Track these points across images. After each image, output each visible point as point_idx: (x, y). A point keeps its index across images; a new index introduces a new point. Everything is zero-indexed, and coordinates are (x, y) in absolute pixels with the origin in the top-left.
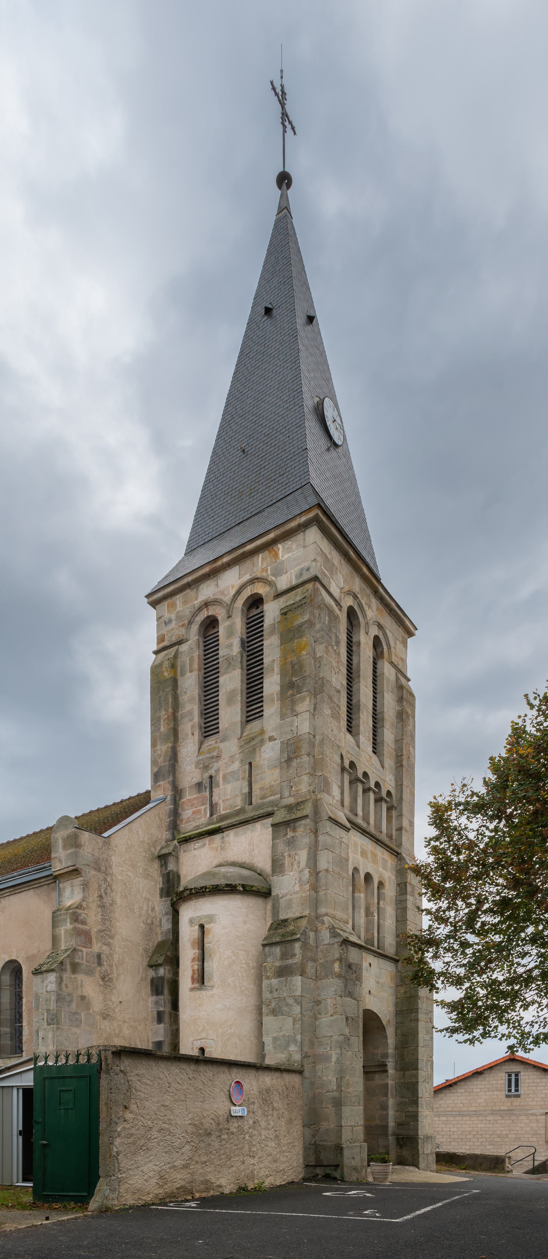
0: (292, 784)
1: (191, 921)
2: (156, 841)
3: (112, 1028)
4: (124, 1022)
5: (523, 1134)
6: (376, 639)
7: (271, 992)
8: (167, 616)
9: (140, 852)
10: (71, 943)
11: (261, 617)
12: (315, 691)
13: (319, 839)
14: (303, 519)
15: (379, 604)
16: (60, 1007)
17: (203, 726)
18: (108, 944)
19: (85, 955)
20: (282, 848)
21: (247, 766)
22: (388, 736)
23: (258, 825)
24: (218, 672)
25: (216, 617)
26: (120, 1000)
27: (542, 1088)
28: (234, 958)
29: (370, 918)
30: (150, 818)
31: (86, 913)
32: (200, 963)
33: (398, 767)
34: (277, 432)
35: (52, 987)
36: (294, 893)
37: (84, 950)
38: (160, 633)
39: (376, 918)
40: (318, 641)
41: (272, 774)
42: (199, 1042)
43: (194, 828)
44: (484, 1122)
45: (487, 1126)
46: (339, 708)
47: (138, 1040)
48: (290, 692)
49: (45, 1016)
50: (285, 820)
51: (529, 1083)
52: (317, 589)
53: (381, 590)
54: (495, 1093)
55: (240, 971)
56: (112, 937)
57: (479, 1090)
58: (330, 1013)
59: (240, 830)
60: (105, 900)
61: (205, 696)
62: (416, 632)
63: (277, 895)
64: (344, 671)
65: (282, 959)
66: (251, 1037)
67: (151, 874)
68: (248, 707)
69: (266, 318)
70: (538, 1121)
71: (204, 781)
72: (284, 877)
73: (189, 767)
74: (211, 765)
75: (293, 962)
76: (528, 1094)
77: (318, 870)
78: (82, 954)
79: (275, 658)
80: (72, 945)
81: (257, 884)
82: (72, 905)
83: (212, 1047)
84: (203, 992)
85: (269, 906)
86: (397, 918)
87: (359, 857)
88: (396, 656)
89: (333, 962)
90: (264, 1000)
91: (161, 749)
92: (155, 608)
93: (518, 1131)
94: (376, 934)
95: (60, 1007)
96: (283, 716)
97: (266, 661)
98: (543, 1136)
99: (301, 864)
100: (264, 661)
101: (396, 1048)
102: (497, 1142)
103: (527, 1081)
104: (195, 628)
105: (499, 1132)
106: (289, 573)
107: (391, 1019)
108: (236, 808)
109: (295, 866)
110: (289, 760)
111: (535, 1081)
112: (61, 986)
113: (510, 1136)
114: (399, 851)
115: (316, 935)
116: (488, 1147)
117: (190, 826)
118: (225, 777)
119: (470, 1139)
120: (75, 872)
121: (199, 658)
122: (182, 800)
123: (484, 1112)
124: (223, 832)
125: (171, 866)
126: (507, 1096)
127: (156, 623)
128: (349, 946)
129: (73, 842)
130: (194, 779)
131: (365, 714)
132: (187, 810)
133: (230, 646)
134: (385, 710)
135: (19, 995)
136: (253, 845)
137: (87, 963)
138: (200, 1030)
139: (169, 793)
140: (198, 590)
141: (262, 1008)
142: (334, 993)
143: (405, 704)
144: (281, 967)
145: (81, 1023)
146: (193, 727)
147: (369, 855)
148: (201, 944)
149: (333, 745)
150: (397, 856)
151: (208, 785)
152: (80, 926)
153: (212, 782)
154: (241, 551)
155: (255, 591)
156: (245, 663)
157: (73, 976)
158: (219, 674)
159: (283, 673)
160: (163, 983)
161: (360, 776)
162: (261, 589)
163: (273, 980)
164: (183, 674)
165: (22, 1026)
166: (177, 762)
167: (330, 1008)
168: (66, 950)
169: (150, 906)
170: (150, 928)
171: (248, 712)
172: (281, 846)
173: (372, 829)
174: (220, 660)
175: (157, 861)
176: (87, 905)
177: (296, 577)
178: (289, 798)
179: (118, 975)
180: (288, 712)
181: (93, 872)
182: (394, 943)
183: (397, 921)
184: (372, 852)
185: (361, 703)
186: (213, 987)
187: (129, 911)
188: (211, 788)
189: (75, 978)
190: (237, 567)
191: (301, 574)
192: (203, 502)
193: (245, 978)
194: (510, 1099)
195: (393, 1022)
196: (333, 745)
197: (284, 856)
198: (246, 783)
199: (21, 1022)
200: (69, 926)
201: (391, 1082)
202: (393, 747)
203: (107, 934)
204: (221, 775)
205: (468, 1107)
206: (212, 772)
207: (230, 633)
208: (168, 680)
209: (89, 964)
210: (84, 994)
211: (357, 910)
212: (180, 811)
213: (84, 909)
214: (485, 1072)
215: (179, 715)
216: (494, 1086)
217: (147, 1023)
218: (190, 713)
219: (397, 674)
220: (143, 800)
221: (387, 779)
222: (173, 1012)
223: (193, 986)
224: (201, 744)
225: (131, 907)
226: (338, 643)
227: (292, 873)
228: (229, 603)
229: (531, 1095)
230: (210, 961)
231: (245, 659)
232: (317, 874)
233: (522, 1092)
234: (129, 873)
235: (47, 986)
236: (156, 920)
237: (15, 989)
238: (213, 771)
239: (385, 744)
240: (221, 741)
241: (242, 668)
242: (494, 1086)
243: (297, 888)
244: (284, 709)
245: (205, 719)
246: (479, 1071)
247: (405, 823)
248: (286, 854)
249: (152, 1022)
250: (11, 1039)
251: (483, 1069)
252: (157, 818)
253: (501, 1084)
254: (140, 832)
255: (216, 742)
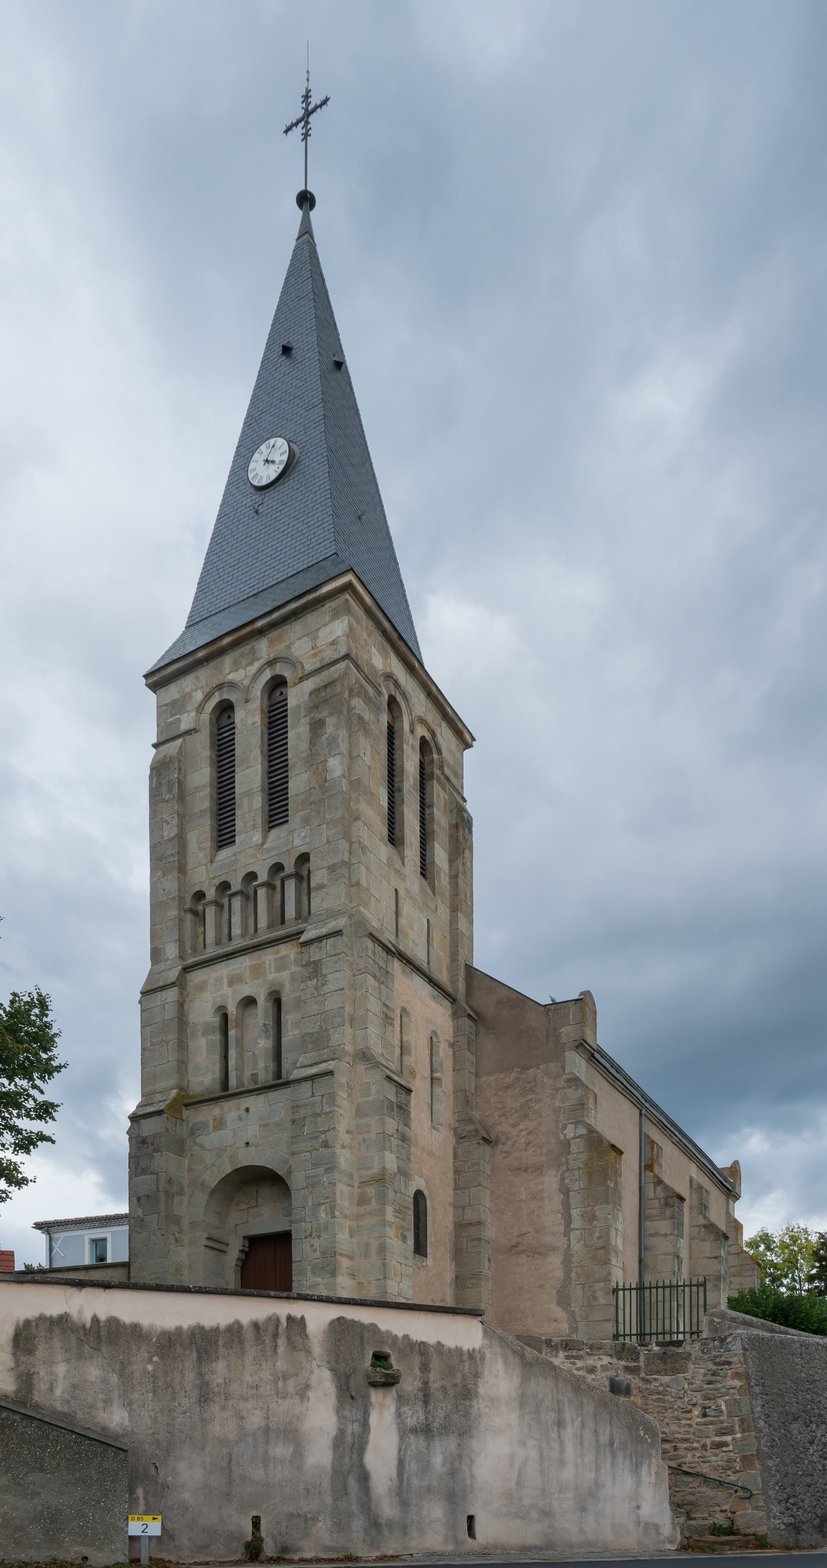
6: (423, 742)
22: (440, 855)
34: (291, 549)
52: (350, 669)
69: (284, 358)
92: (155, 692)
150: (452, 1003)
192: (201, 597)
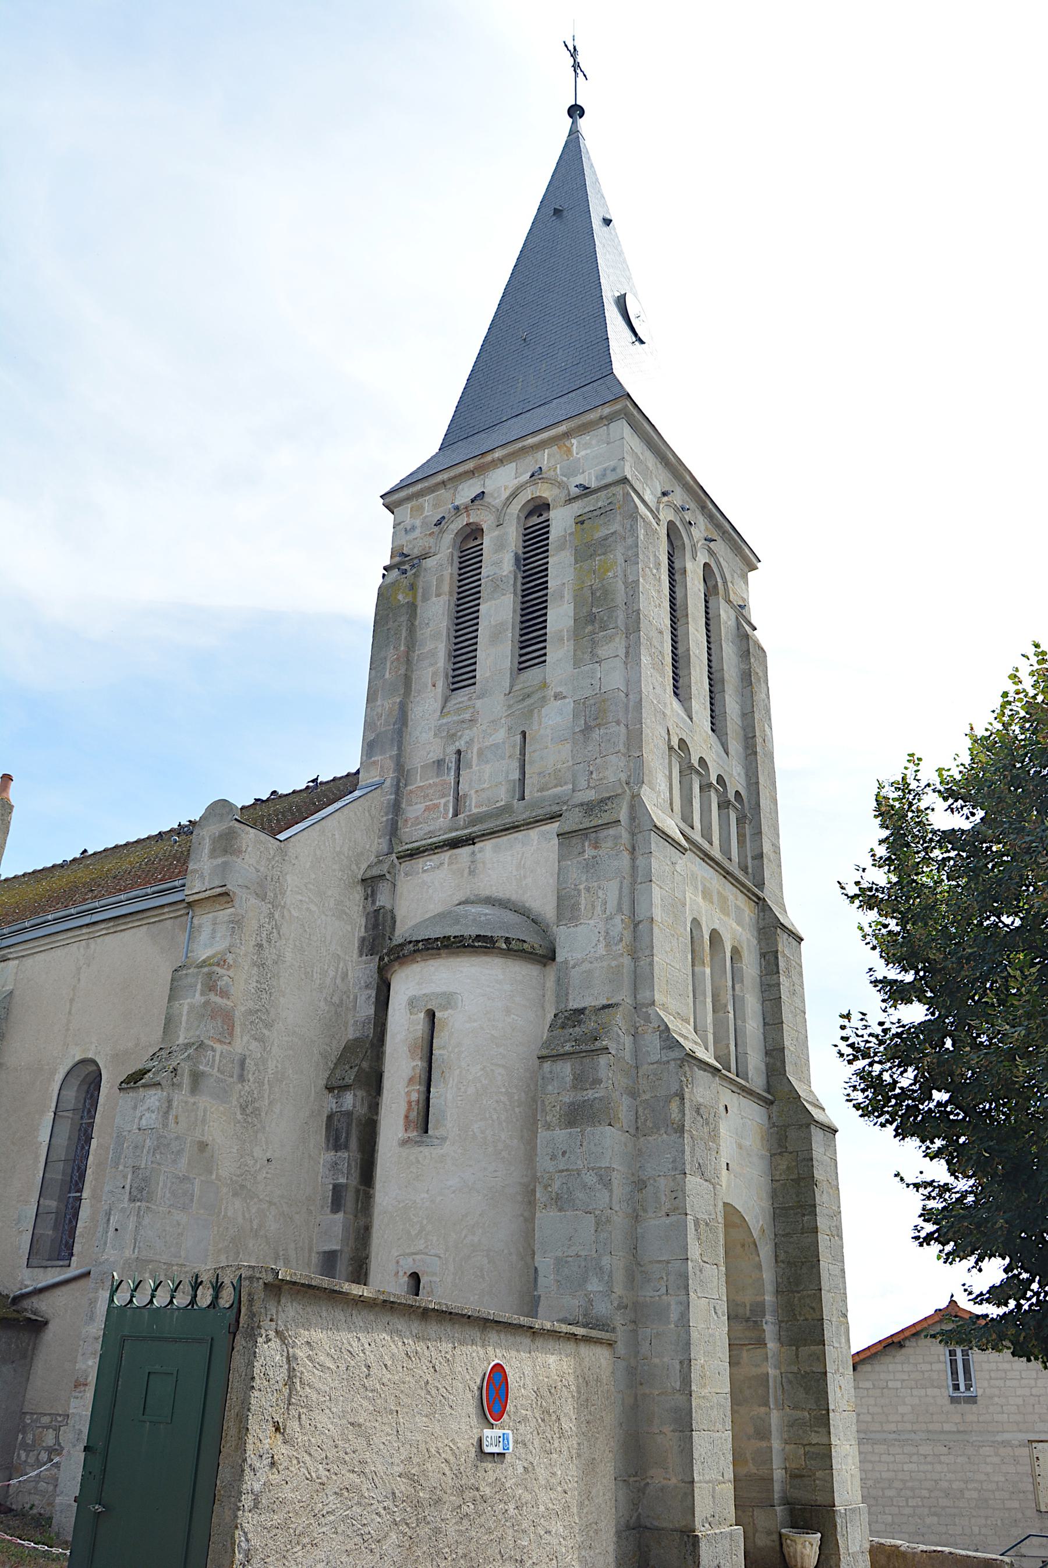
0: (591, 768)
1: (412, 1003)
2: (362, 854)
3: (247, 1216)
4: (271, 1203)
5: (993, 1491)
7: (553, 1157)
8: (408, 522)
9: (334, 870)
10: (198, 1033)
11: (546, 526)
12: (627, 629)
13: (638, 862)
14: (607, 410)
15: (708, 524)
16: (159, 1164)
17: (451, 673)
18: (261, 1039)
19: (217, 1058)
20: (575, 876)
21: (518, 738)
22: (732, 705)
23: (534, 834)
24: (479, 598)
25: (481, 525)
26: (268, 1155)
27: (1014, 1383)
28: (485, 1082)
29: (721, 1014)
30: (355, 814)
31: (232, 975)
32: (423, 1089)
33: (750, 755)
35: (150, 1119)
36: (597, 959)
37: (218, 1047)
38: (396, 544)
39: (731, 1015)
40: (630, 561)
41: (559, 752)
42: (410, 1260)
43: (425, 834)
44: (915, 1458)
45: (922, 1468)
46: (663, 656)
47: (292, 1246)
48: (590, 628)
49: (129, 1180)
50: (581, 827)
51: (990, 1371)
52: (628, 494)
53: (711, 506)
54: (929, 1391)
55: (495, 1109)
56: (269, 1026)
57: (898, 1384)
58: (665, 1209)
59: (504, 840)
60: (266, 953)
61: (457, 631)
62: (759, 565)
63: (566, 962)
64: (667, 604)
65: (574, 1087)
66: (510, 1254)
67: (348, 911)
68: (522, 648)
70: (1016, 1461)
71: (447, 758)
72: (579, 929)
73: (424, 735)
74: (459, 734)
75: (596, 1095)
76: (991, 1397)
77: (637, 919)
78: (214, 1056)
79: (565, 581)
80: (199, 1036)
81: (533, 940)
82: (209, 958)
83: (434, 1274)
84: (425, 1150)
85: (551, 983)
86: (764, 1019)
87: (700, 900)
88: (735, 593)
89: (668, 1100)
90: (539, 1174)
91: (383, 705)
93: (981, 1482)
94: (732, 1048)
95: (159, 1164)
96: (577, 663)
97: (552, 584)
98: (1031, 1497)
99: (608, 906)
100: (549, 585)
101: (778, 1292)
102: (944, 1508)
103: (985, 1366)
104: (448, 538)
105: (944, 1485)
106: (586, 473)
107: (765, 1226)
108: (498, 805)
109: (598, 910)
110: (587, 729)
111: (1002, 1366)
112: (167, 1118)
113: (967, 1494)
114: (759, 893)
115: (635, 1042)
116: (928, 1521)
117: (419, 832)
118: (480, 753)
119: (891, 1498)
120: (224, 896)
121: (451, 578)
122: (409, 788)
123: (913, 1436)
124: (474, 844)
125: (383, 900)
126: (954, 1400)
127: (392, 530)
128: (695, 1068)
129: (226, 844)
130: (431, 754)
131: (698, 669)
132: (416, 803)
133: (498, 563)
134: (725, 668)
135: (86, 1131)
136: (524, 867)
137: (219, 1075)
138: (413, 1233)
139: (390, 776)
140: (456, 490)
141: (534, 1191)
142: (670, 1166)
143: (752, 660)
144: (572, 1104)
145: (192, 1200)
146: (434, 674)
147: (715, 898)
148: (426, 1050)
149: (655, 710)
151: (453, 766)
152: (218, 999)
153: (459, 760)
154: (520, 445)
155: (538, 494)
156: (519, 587)
157: (192, 1100)
158: (480, 601)
159: (578, 601)
160: (349, 1125)
161: (695, 763)
162: (545, 492)
163: (558, 1132)
164: (425, 599)
165: (80, 1199)
166: (407, 727)
167: (663, 1198)
168: (187, 1046)
169: (340, 970)
170: (336, 1013)
171: (521, 656)
172: (574, 874)
173: (716, 852)
174: (482, 581)
175: (359, 888)
176: (235, 961)
177: (597, 478)
178: (588, 791)
179: (270, 1103)
180: (586, 656)
181: (253, 901)
182: (763, 1067)
183: (765, 1024)
184: (719, 893)
185: (691, 653)
186: (444, 1139)
187: (303, 977)
188: (458, 769)
189: (194, 1104)
190: (514, 464)
191: (604, 475)
193: (504, 1124)
194: (959, 1407)
195: (769, 1234)
196: (655, 710)
197: (579, 891)
198: (516, 764)
199: (81, 1191)
200: (198, 998)
201: (771, 1371)
202: (740, 723)
203: (261, 1019)
204: (475, 750)
205: (881, 1423)
206: (461, 744)
207: (500, 546)
208: (403, 605)
209: (221, 1076)
210: (205, 1139)
211: (700, 998)
212: (403, 806)
213: (229, 967)
214: (907, 1343)
215: (415, 656)
216: (926, 1375)
217: (312, 1208)
218: (433, 653)
219: (737, 618)
220: (347, 784)
221: (735, 774)
222: (362, 1188)
223: (406, 1135)
224: (446, 700)
225: (309, 970)
226: (658, 565)
227: (592, 922)
228: (500, 508)
229: (996, 1399)
230: (442, 1085)
231: (520, 581)
232: (636, 925)
233: (980, 1392)
234: (313, 908)
235: (141, 1118)
236: (348, 997)
237: (82, 1118)
238: (462, 743)
239: (728, 718)
240: (478, 698)
241: (515, 594)
242: (926, 1375)
243: (601, 950)
244: (579, 653)
245: (454, 664)
246: (896, 1340)
247: (767, 848)
248: (582, 887)
249: (322, 1207)
250: (55, 1228)
251: (902, 1336)
252: (367, 814)
253: (938, 1371)
254: (337, 836)
255: (470, 699)
